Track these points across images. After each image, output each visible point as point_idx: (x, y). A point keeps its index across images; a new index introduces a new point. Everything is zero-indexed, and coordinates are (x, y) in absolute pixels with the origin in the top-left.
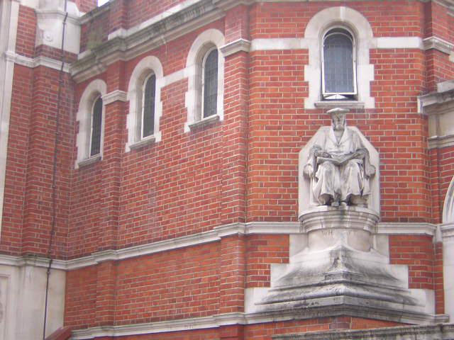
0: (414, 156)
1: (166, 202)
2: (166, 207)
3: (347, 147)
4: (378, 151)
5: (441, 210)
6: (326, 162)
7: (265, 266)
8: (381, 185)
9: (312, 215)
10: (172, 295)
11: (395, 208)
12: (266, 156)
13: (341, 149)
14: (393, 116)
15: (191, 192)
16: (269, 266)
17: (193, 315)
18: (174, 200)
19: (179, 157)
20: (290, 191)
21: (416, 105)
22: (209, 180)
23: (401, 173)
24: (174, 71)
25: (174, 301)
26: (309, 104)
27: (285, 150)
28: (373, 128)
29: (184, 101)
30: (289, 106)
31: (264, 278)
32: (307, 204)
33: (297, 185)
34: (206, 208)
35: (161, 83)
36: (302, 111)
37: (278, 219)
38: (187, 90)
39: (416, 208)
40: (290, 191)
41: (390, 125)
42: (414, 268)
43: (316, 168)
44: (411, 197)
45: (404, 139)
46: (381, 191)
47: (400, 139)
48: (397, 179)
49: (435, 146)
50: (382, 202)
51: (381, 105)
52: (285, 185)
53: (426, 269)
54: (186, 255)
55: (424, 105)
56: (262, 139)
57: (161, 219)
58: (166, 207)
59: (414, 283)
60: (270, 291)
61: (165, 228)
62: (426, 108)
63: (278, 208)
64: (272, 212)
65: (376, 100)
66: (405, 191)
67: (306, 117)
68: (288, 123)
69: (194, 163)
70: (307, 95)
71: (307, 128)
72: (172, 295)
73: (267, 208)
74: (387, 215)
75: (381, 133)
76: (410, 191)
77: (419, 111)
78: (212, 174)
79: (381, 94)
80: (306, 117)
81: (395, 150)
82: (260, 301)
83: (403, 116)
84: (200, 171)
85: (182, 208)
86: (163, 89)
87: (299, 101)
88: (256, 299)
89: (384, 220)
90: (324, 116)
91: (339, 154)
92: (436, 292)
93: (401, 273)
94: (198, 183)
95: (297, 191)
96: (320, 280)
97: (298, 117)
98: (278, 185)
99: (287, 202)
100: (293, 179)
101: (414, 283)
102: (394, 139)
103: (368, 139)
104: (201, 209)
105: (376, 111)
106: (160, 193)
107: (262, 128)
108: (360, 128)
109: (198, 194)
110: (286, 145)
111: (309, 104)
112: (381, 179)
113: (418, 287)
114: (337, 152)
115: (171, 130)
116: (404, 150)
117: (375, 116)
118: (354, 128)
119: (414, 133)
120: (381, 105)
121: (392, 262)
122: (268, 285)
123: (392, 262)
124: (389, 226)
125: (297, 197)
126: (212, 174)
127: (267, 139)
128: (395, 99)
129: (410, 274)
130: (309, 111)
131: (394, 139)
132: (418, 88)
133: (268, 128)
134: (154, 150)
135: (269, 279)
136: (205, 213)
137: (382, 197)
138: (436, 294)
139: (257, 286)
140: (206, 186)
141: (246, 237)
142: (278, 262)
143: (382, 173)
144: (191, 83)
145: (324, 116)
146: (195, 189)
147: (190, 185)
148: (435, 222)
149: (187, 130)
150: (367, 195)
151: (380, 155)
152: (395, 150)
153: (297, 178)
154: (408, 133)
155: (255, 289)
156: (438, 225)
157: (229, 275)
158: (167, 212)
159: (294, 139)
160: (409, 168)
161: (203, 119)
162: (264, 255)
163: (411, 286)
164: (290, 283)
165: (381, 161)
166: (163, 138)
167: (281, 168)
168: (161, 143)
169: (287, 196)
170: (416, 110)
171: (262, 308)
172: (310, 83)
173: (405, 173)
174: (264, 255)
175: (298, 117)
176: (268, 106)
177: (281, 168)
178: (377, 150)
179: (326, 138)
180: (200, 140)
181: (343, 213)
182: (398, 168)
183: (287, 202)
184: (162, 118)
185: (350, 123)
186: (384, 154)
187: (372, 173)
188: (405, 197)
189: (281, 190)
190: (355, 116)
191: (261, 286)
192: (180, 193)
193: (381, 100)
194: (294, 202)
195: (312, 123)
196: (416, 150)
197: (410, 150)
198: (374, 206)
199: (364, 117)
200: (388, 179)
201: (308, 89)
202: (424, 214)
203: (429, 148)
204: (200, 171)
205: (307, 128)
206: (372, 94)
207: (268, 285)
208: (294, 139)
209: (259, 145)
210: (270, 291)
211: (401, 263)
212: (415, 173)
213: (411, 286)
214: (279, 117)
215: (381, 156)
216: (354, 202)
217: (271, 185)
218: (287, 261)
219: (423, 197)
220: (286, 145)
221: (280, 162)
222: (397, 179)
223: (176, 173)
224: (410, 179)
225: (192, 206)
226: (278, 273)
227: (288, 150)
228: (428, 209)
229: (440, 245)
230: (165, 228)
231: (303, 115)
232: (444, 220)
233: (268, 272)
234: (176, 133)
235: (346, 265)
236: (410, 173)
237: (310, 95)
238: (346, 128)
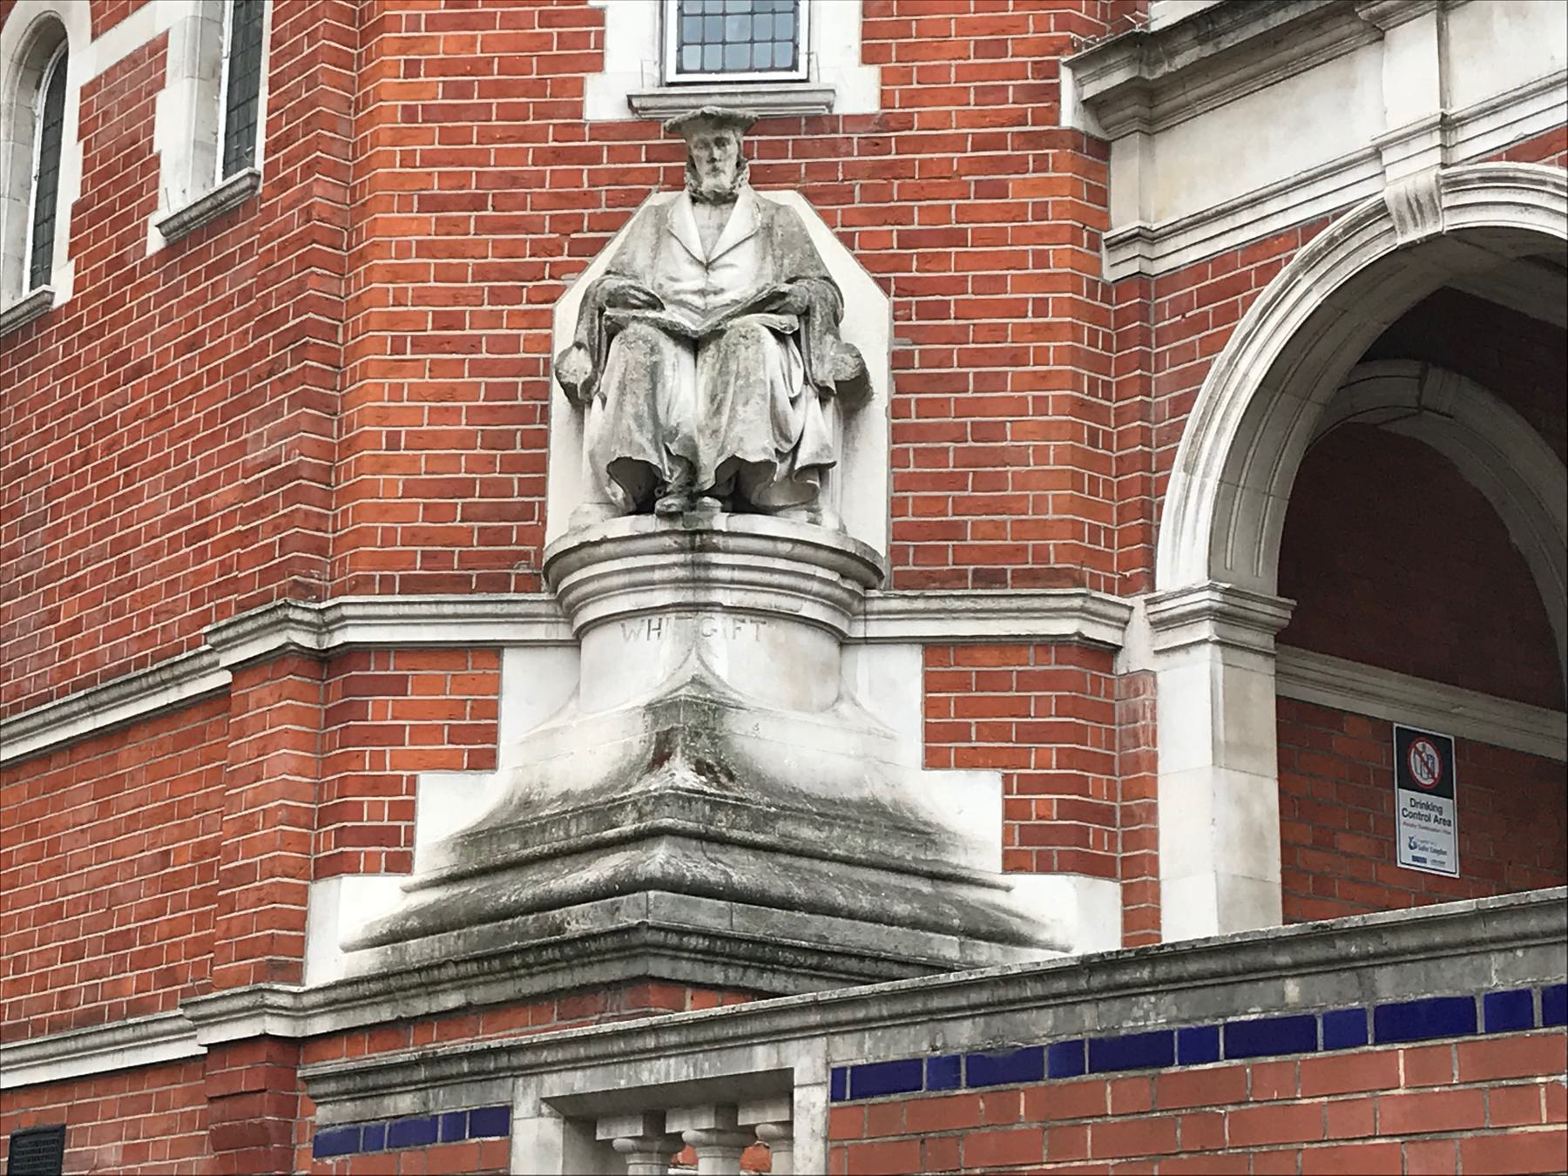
0: (1040, 307)
1: (74, 544)
2: (74, 565)
3: (742, 276)
4: (887, 292)
5: (1149, 536)
6: (634, 327)
7: (391, 786)
8: (897, 434)
9: (583, 552)
10: (74, 929)
11: (955, 531)
12: (417, 321)
13: (718, 278)
14: (957, 143)
15: (156, 496)
16: (413, 782)
17: (136, 1008)
18: (100, 533)
19: (125, 357)
20: (511, 465)
21: (1054, 92)
22: (216, 438)
23: (982, 382)
24: (124, 14)
25: (75, 952)
26: (603, 101)
27: (496, 296)
28: (869, 193)
29: (150, 127)
30: (519, 113)
31: (387, 836)
32: (573, 506)
33: (542, 439)
34: (201, 555)
35: (86, 61)
36: (574, 130)
37: (459, 584)
38: (161, 85)
39: (1043, 529)
40: (511, 465)
41: (942, 180)
42: (1027, 784)
43: (598, 357)
44: (1022, 482)
45: (999, 237)
46: (896, 459)
47: (980, 238)
48: (964, 408)
49: (1132, 268)
50: (896, 507)
51: (910, 99)
52: (491, 441)
53: (1080, 786)
54: (129, 758)
55: (1090, 91)
56: (403, 251)
57: (53, 616)
58: (74, 565)
59: (1030, 849)
60: (408, 891)
61: (65, 652)
62: (1093, 106)
63: (463, 537)
64: (434, 555)
65: (886, 77)
66: (1001, 458)
67: (592, 156)
68: (514, 180)
69: (169, 376)
70: (597, 64)
71: (589, 199)
72: (74, 929)
73: (412, 537)
74: (926, 555)
75: (903, 216)
76: (1020, 457)
77: (1069, 116)
78: (226, 413)
79: (906, 52)
80: (592, 156)
81: (958, 285)
82: (355, 930)
83: (998, 142)
84: (188, 405)
85: (124, 565)
86: (87, 91)
87: (560, 87)
88: (349, 921)
89: (903, 582)
90: (673, 146)
91: (713, 300)
92: (1126, 890)
93: (969, 809)
94: (181, 455)
95: (541, 464)
96: (580, 832)
97: (558, 156)
98: (465, 441)
99: (499, 512)
100: (526, 415)
101: (1030, 849)
102: (958, 238)
103: (847, 240)
104: (183, 562)
105: (884, 122)
106: (56, 511)
107: (405, 205)
108: (811, 196)
109: (177, 499)
110: (505, 273)
111: (603, 101)
112: (897, 409)
113: (1045, 867)
114: (702, 293)
115: (105, 251)
116: (998, 283)
117: (878, 146)
118: (790, 199)
119: (1040, 211)
120: (910, 99)
121: (934, 760)
122: (401, 864)
123: (934, 760)
124: (920, 604)
125: (540, 488)
126: (226, 413)
127: (425, 249)
128: (964, 74)
129: (1011, 811)
130: (603, 130)
131: (958, 238)
132: (1064, 23)
133: (428, 204)
134: (47, 340)
135: (410, 841)
136: (201, 576)
137: (900, 483)
138: (1128, 896)
139: (354, 871)
140: (207, 464)
141: (327, 662)
142: (449, 764)
143: (900, 384)
144: (178, 56)
145: (673, 146)
146: (171, 481)
147: (154, 469)
148: (1128, 588)
149: (155, 242)
150: (821, 470)
151: (896, 306)
152: (958, 285)
153: (546, 410)
154: (1018, 213)
155: (348, 881)
156: (1138, 601)
157: (248, 825)
158: (75, 587)
159: (539, 248)
160: (1017, 358)
161: (219, 183)
162: (393, 735)
163: (1012, 863)
164: (488, 853)
165: (898, 332)
166: (78, 286)
167: (478, 368)
168: (71, 305)
169: (503, 488)
170: (1053, 114)
171: (367, 962)
172: (610, 17)
173: (998, 381)
174: (393, 735)
175: (558, 156)
176: (430, 113)
177: (478, 368)
178: (883, 284)
179: (701, 248)
180: (193, 281)
181: (698, 542)
182: (968, 359)
183: (499, 512)
184: (77, 209)
185: (761, 179)
186: (916, 305)
187: (848, 372)
188: (998, 482)
189: (475, 464)
190: (788, 142)
191: (372, 870)
192: (125, 501)
193: (906, 77)
194: (526, 512)
195: (616, 177)
196: (1050, 282)
197: (1022, 284)
198: (861, 509)
199: (833, 148)
200: (924, 408)
201: (601, 36)
202: (1073, 553)
203: (1109, 275)
204: (188, 405)
205: (589, 199)
206: (869, 56)
207: (401, 864)
208: (539, 248)
209: (395, 274)
210: (408, 891)
211: (970, 761)
212: (1042, 380)
213: (1012, 863)
214: (480, 158)
215: (898, 312)
216: (754, 499)
217: (436, 440)
218: (485, 761)
219: (1076, 481)
220: (505, 273)
221: (473, 345)
222: (964, 408)
223: (110, 426)
224: (1019, 407)
225: (156, 552)
226: (448, 807)
227: (513, 296)
228: (1094, 530)
229: (1141, 682)
230: (65, 652)
231: (578, 145)
232: (1164, 583)
233: (407, 811)
234: (119, 262)
235: (701, 768)
236: (1021, 383)
237: (609, 62)
238: (746, 194)
